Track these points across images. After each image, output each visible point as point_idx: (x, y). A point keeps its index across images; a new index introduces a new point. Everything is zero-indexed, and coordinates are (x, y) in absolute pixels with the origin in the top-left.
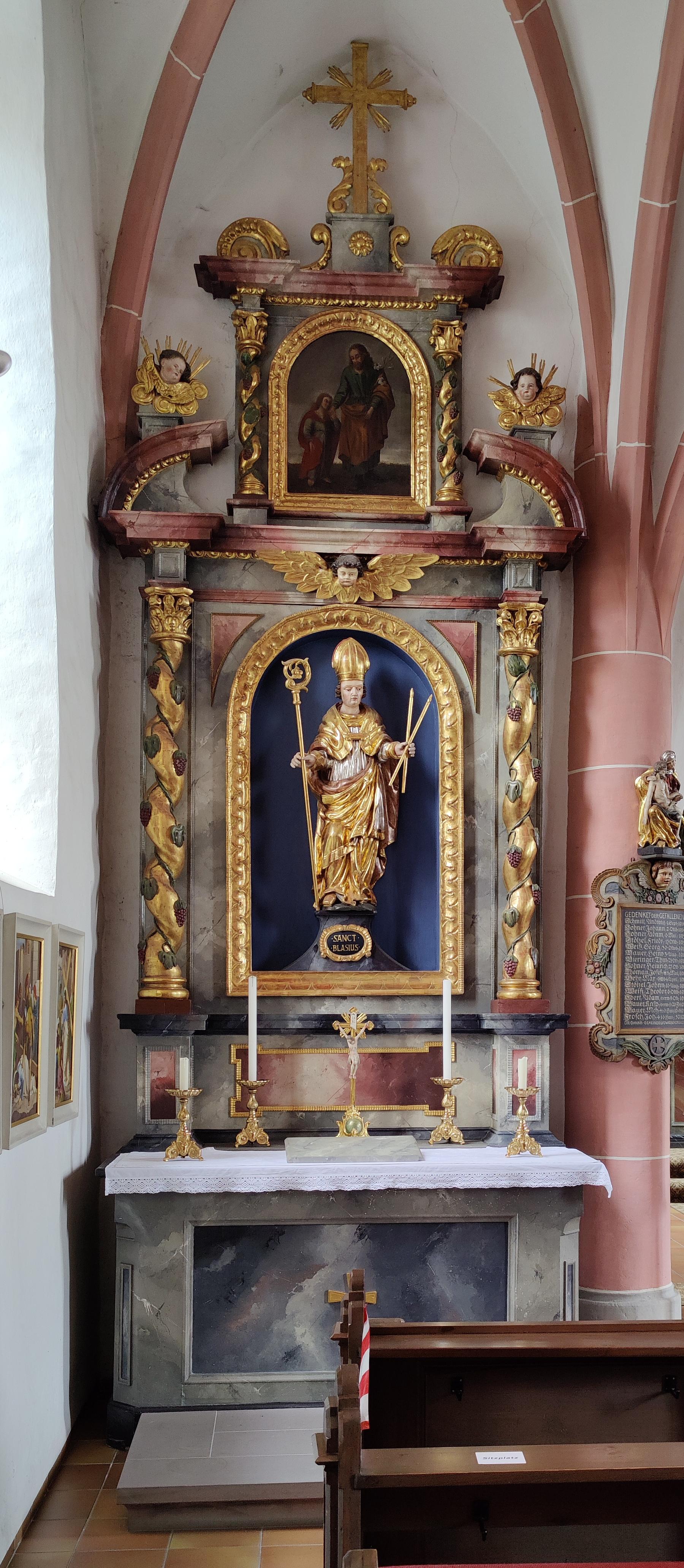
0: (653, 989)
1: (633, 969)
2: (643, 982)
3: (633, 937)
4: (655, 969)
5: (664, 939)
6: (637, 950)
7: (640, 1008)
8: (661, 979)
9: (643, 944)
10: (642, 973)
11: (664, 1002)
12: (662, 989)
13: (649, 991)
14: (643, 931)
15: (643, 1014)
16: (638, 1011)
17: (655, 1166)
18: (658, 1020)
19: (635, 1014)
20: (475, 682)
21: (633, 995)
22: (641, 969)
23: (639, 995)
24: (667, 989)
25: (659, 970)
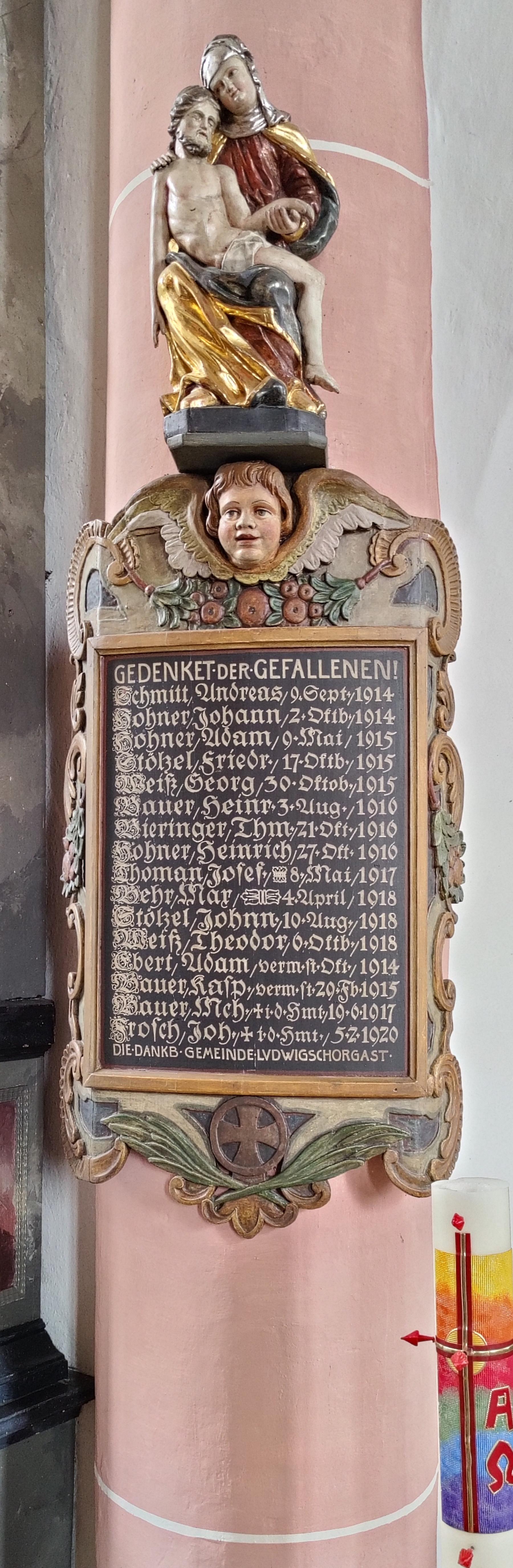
0: (224, 932)
1: (141, 864)
2: (180, 907)
3: (143, 751)
4: (234, 863)
5: (278, 753)
6: (156, 796)
7: (168, 998)
8: (262, 897)
9: (181, 775)
10: (178, 875)
11: (271, 979)
12: (262, 932)
13: (207, 940)
14: (180, 728)
15: (178, 1019)
16: (161, 1009)
17: (120, 603)
18: (241, 1044)
19: (149, 1019)
20: (431, 776)
21: (144, 953)
22: (173, 864)
23: (164, 953)
24: (291, 933)
25: (253, 863)
